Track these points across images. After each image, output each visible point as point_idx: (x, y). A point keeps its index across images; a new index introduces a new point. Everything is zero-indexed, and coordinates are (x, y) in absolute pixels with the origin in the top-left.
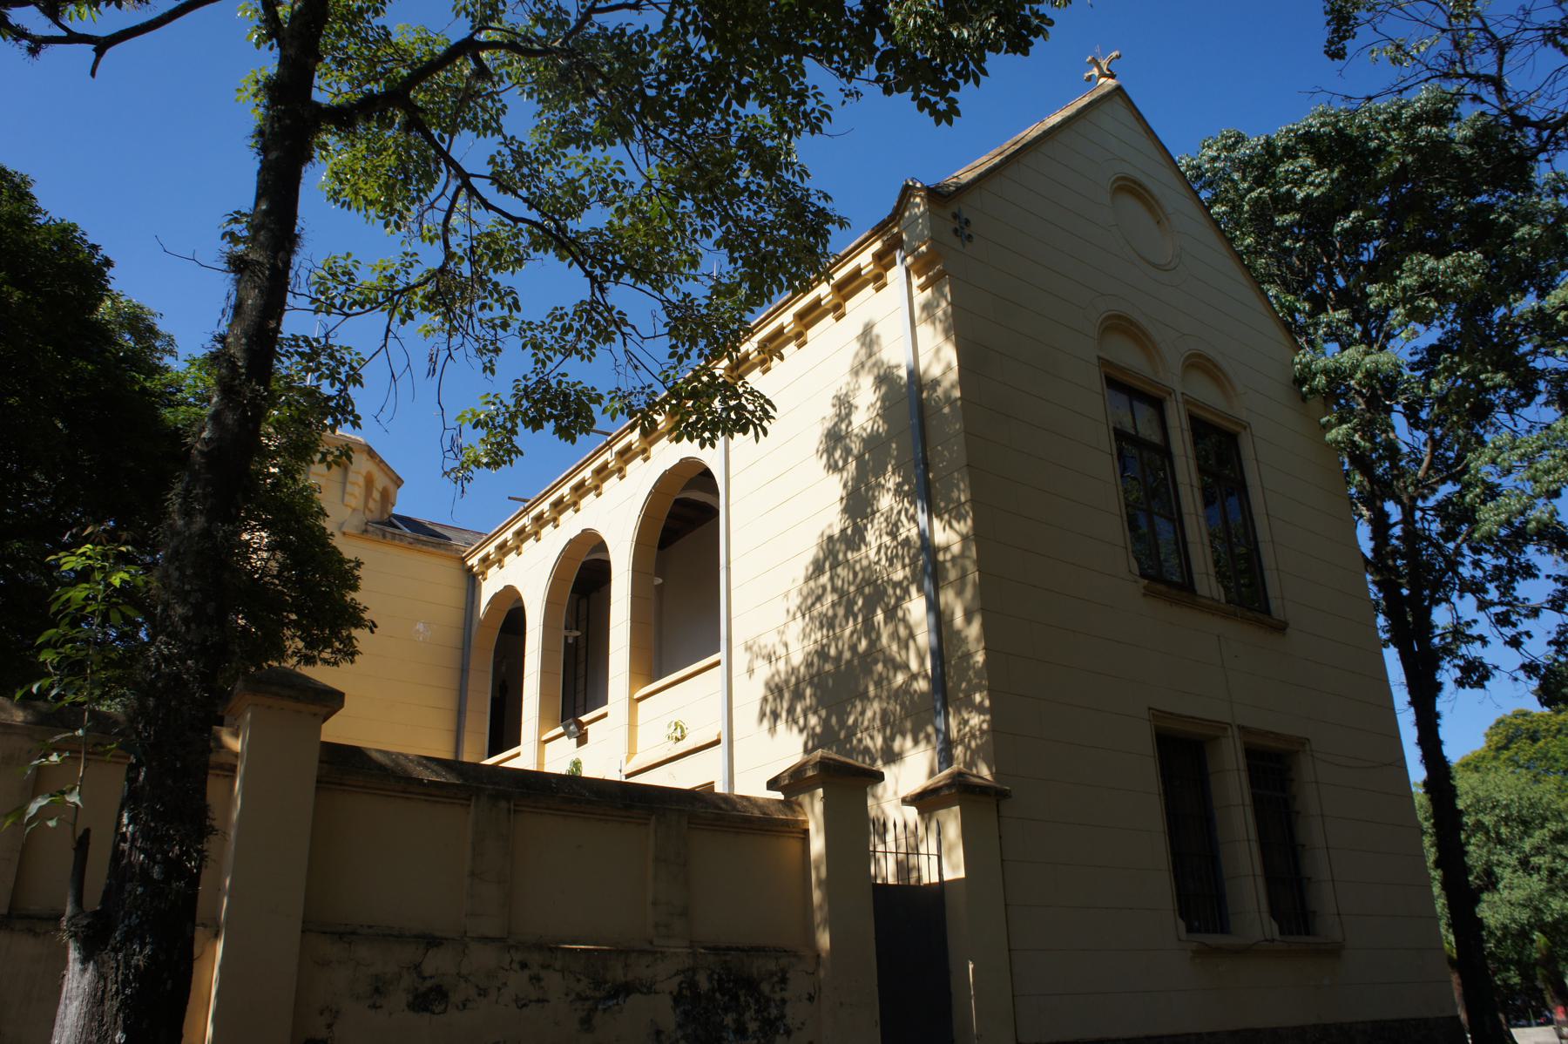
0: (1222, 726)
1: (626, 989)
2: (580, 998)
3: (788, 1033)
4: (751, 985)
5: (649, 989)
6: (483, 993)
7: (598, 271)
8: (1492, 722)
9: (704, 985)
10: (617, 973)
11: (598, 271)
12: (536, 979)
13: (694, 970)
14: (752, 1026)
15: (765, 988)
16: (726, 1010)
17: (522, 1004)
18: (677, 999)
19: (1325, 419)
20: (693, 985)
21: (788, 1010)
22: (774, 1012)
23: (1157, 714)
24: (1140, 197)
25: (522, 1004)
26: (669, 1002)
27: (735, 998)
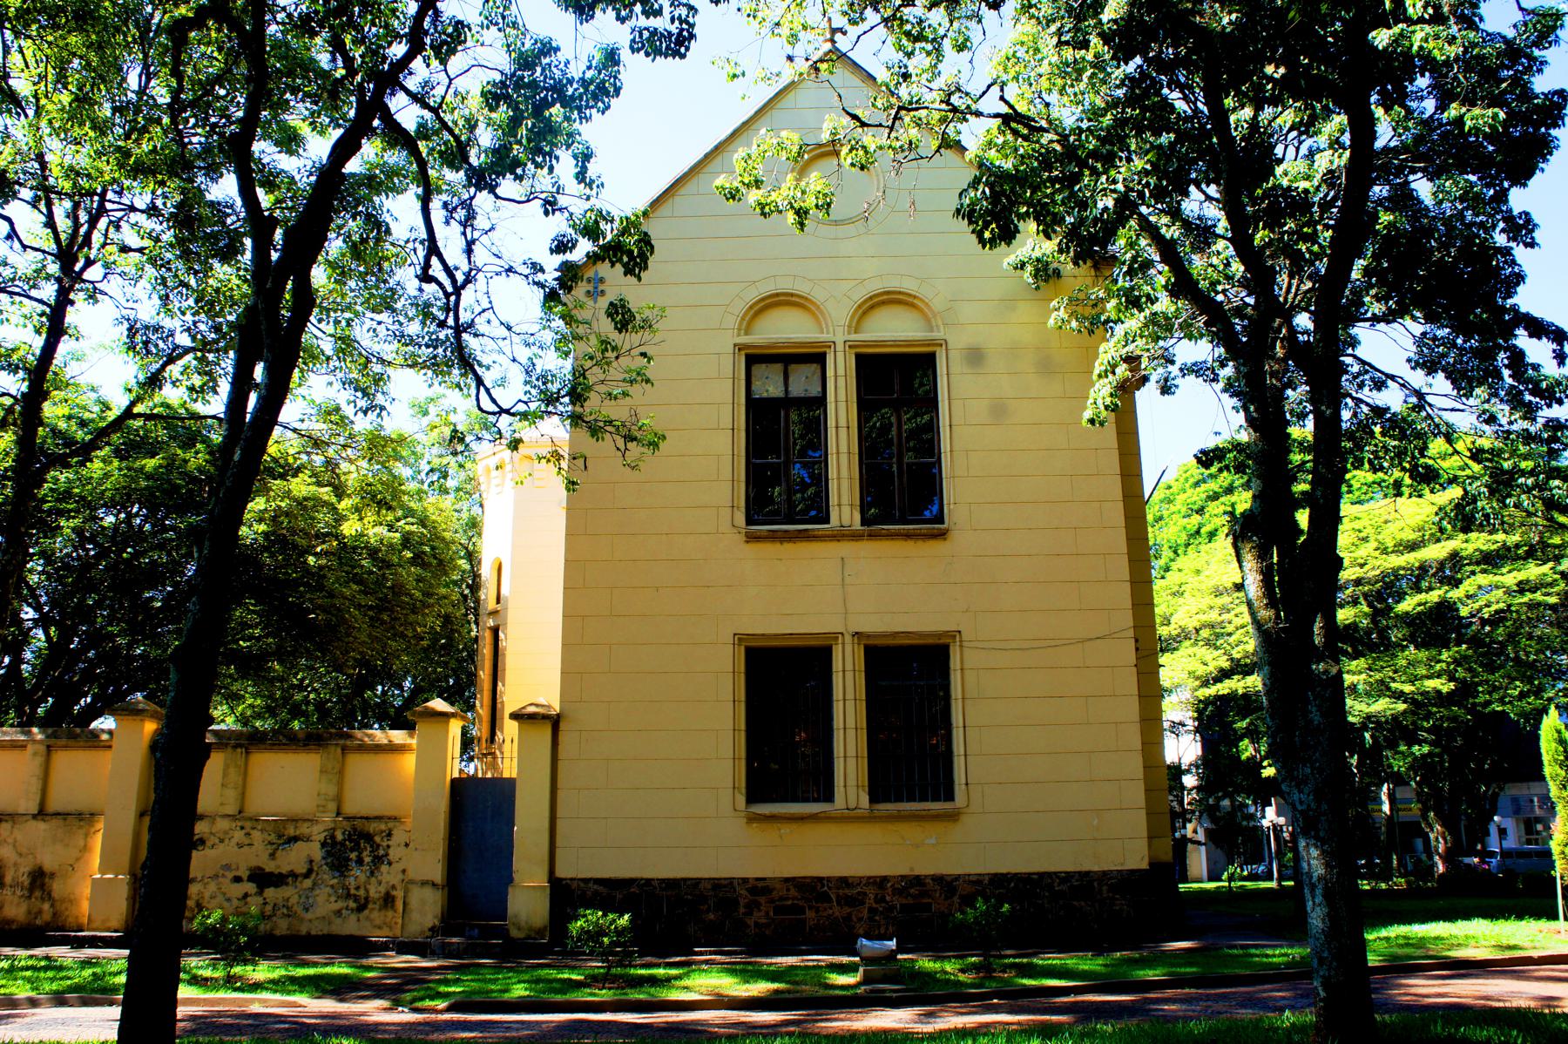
0: (835, 636)
1: (295, 839)
2: (271, 843)
3: (390, 864)
4: (369, 837)
5: (308, 839)
6: (222, 841)
7: (813, 513)
8: (1557, 87)
9: (339, 837)
10: (291, 831)
11: (813, 513)
12: (248, 834)
13: (334, 829)
14: (367, 860)
15: (377, 839)
16: (352, 850)
17: (240, 846)
18: (324, 845)
19: (1051, 322)
20: (333, 837)
21: (391, 852)
22: (381, 852)
23: (740, 638)
24: (899, 302)
25: (240, 846)
26: (318, 845)
27: (358, 844)
